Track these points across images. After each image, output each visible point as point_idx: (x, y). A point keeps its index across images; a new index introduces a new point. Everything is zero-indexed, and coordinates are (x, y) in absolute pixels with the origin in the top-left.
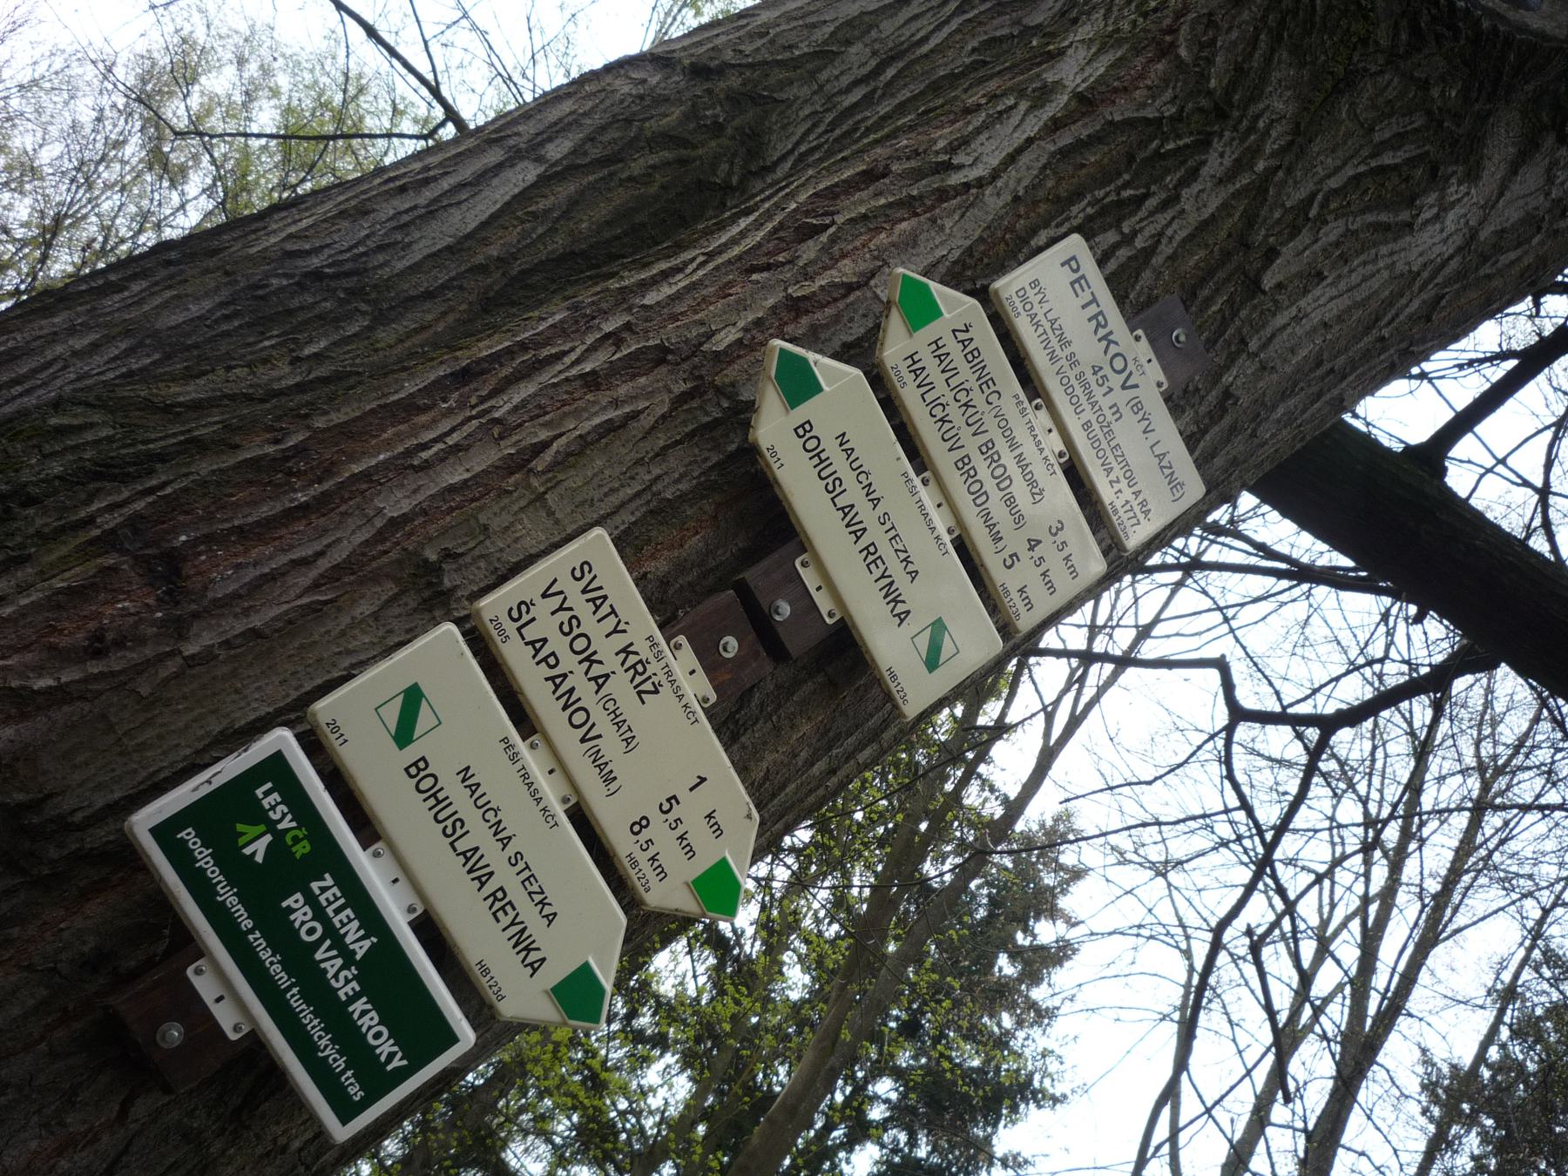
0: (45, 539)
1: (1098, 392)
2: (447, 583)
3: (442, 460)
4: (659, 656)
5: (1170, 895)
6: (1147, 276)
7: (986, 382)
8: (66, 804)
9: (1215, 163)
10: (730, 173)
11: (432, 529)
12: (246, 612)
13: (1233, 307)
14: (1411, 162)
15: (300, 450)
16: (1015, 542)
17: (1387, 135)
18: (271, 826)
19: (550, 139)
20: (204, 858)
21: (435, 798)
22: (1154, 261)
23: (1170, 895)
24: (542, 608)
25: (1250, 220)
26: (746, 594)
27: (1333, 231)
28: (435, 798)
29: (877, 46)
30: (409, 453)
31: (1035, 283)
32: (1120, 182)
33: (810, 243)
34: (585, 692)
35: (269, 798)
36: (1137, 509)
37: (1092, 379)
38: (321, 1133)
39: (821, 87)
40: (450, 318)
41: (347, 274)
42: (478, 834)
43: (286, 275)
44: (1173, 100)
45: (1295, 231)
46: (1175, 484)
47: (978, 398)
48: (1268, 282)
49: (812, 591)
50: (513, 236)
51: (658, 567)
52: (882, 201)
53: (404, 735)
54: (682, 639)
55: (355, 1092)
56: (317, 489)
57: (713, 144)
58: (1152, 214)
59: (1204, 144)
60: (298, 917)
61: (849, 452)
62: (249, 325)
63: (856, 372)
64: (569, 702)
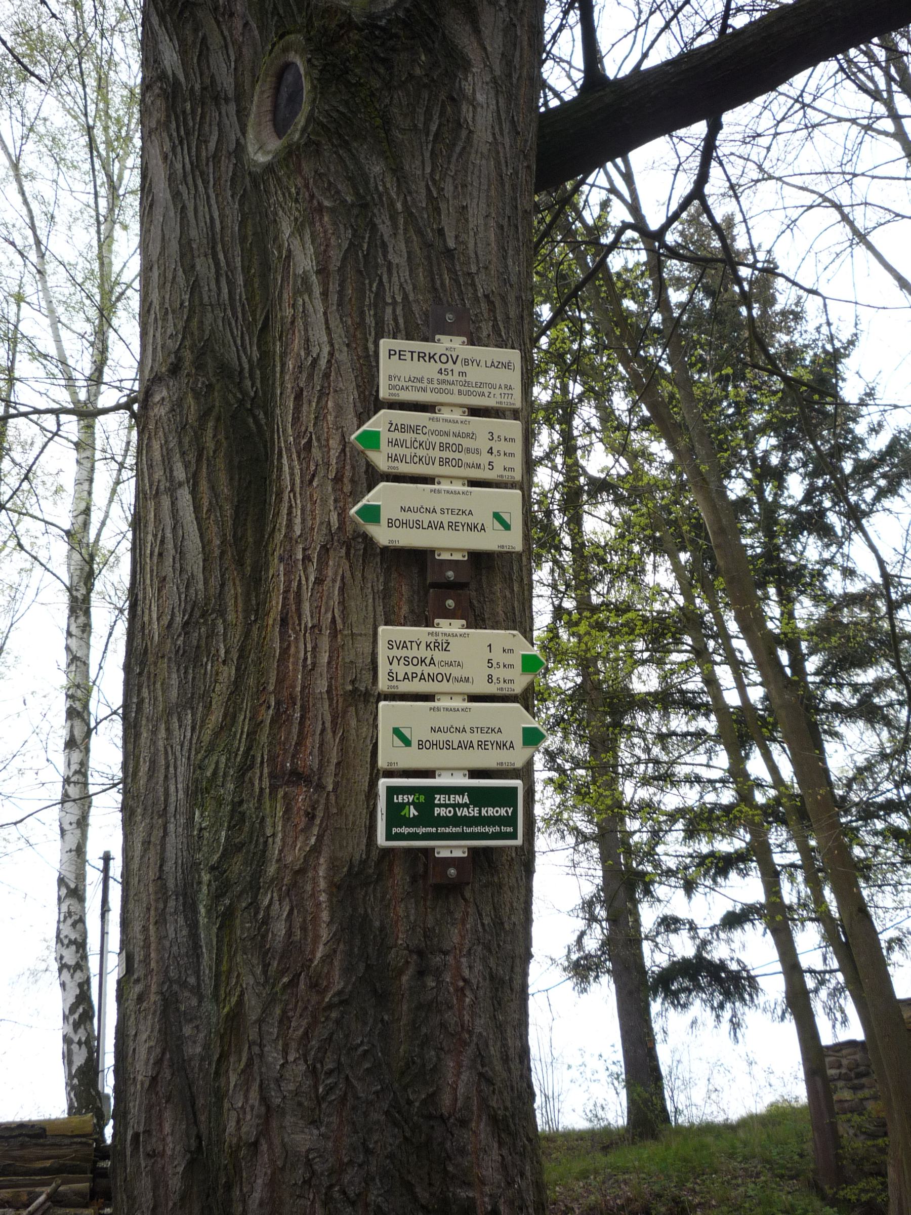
0: (259, 806)
1: (449, 378)
2: (363, 689)
3: (315, 657)
4: (437, 634)
5: (784, 182)
6: (415, 308)
7: (414, 429)
8: (357, 857)
9: (385, 229)
10: (235, 396)
11: (340, 681)
12: (328, 762)
13: (452, 271)
14: (442, 113)
15: (278, 703)
16: (484, 459)
17: (422, 119)
18: (409, 804)
19: (171, 471)
20: (405, 830)
21: (434, 745)
22: (411, 299)
23: (784, 182)
24: (395, 667)
25: (420, 232)
26: (434, 585)
27: (449, 188)
28: (434, 745)
29: (202, 251)
30: (304, 666)
31: (390, 377)
32: (367, 287)
33: (313, 450)
34: (432, 670)
35: (399, 799)
36: (506, 391)
37: (443, 377)
38: (516, 847)
39: (211, 305)
40: (237, 582)
41: (192, 611)
42: (455, 738)
43: (179, 635)
44: (346, 229)
45: (437, 210)
46: (507, 366)
47: (421, 438)
48: (451, 244)
49: (450, 558)
50: (215, 529)
51: (405, 610)
52: (314, 404)
53: (407, 742)
54: (436, 621)
55: (510, 829)
56: (298, 707)
57: (216, 394)
58: (390, 282)
59: (374, 228)
60: (443, 813)
61: (409, 509)
62: (194, 667)
63: (382, 484)
64: (432, 678)
